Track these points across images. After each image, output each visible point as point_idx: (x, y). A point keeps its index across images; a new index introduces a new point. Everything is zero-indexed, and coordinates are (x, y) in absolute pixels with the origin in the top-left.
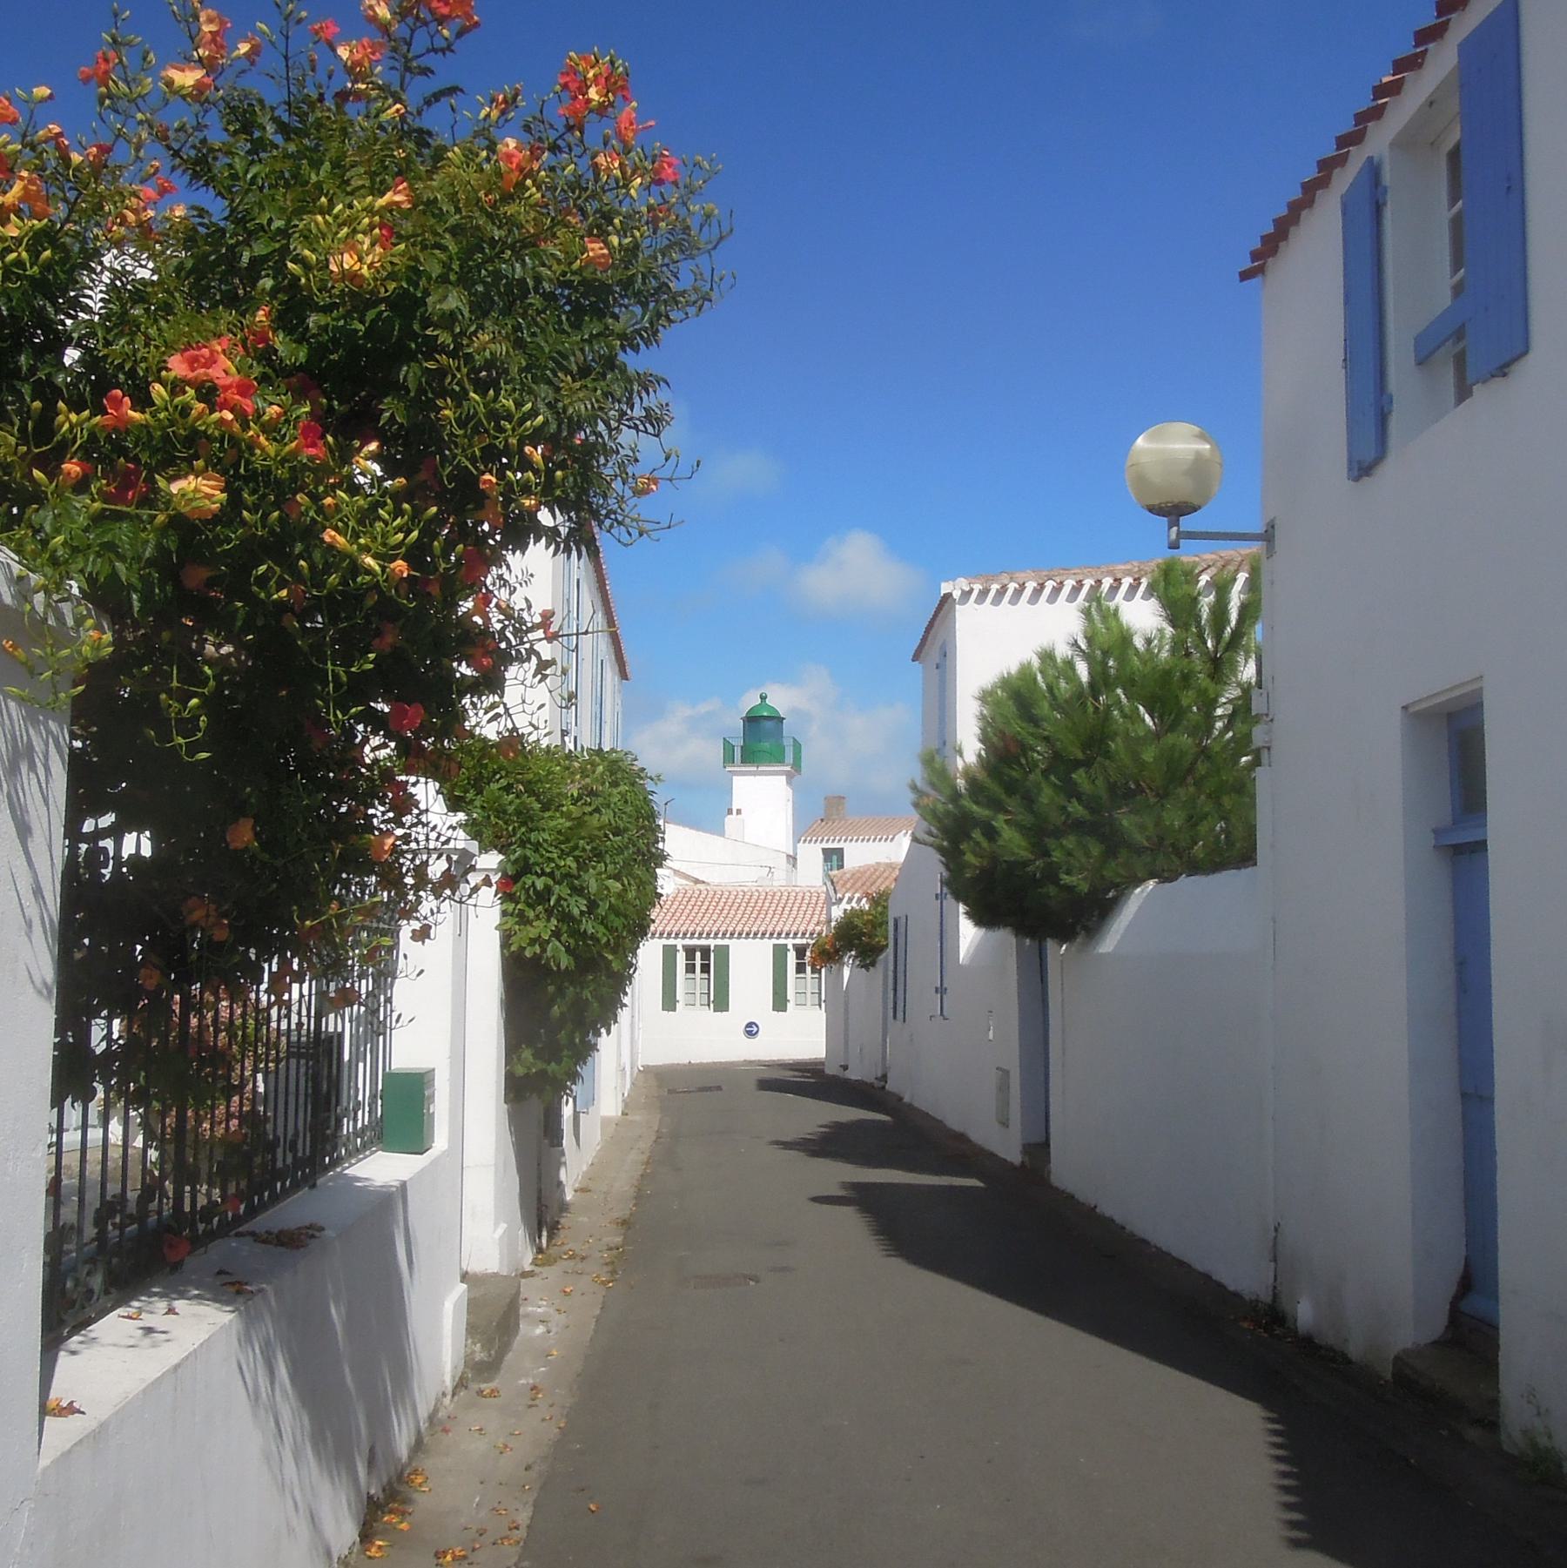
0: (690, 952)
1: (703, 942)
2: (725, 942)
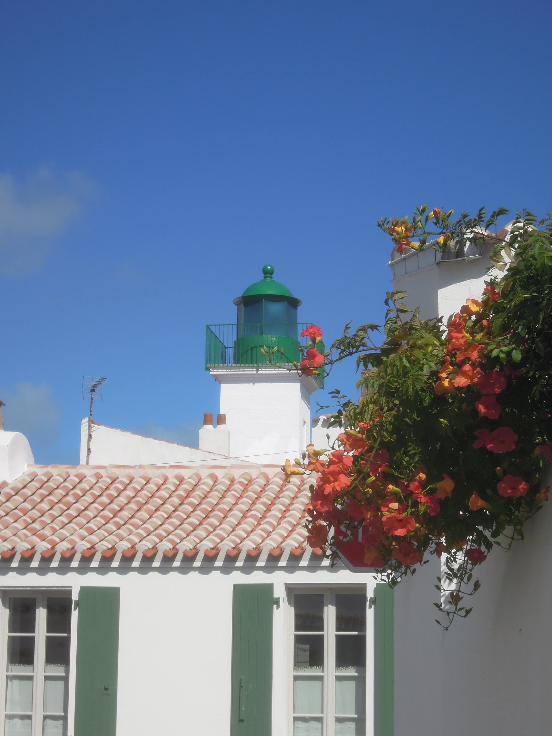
0: (307, 605)
1: (52, 580)
2: (110, 580)
